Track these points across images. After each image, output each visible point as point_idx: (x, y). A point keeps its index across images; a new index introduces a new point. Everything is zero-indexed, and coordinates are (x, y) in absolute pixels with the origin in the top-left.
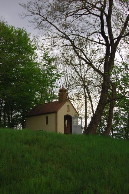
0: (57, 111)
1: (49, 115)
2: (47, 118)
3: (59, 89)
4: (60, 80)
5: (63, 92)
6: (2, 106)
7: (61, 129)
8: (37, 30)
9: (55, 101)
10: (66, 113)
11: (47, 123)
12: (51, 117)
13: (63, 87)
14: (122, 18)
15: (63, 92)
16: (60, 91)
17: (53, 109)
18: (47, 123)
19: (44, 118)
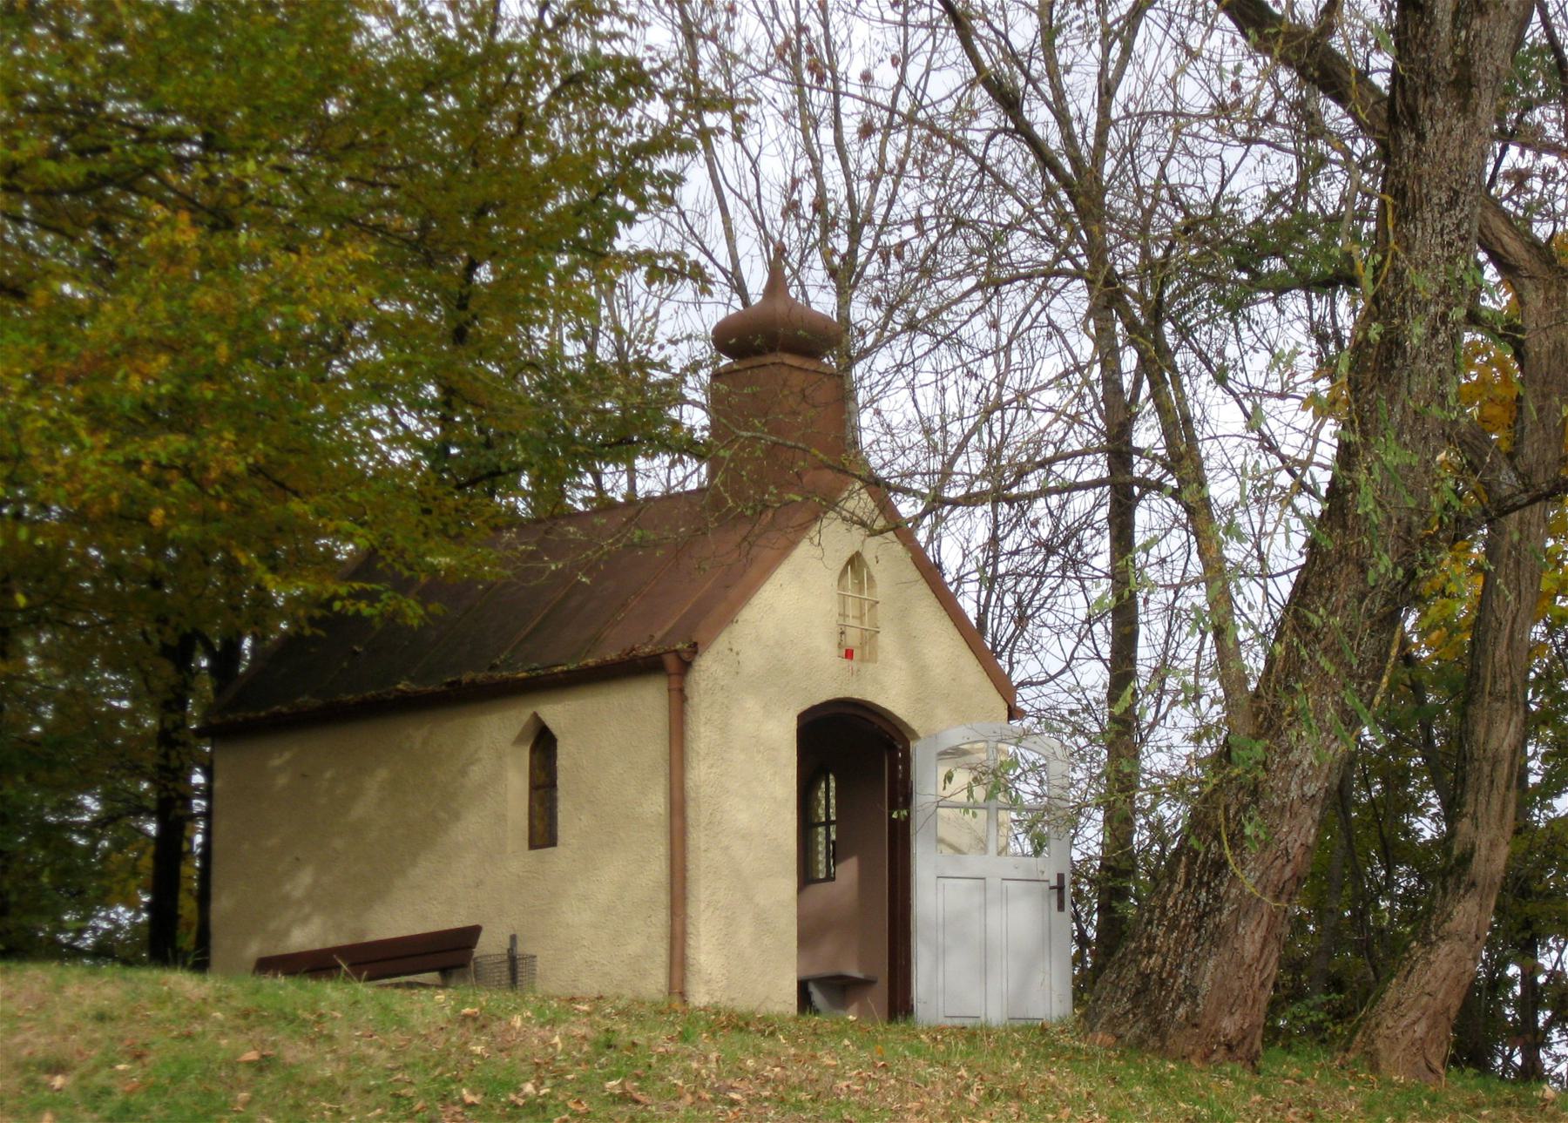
0: (694, 649)
1: (556, 713)
2: (543, 743)
3: (718, 308)
4: (725, 148)
5: (783, 358)
6: (208, 773)
7: (749, 943)
8: (895, 1027)
9: (643, 487)
10: (831, 682)
11: (543, 833)
12: (605, 732)
13: (776, 283)
14: (1467, 685)
15: (783, 358)
16: (730, 339)
17: (625, 628)
18: (543, 833)
19: (492, 746)
